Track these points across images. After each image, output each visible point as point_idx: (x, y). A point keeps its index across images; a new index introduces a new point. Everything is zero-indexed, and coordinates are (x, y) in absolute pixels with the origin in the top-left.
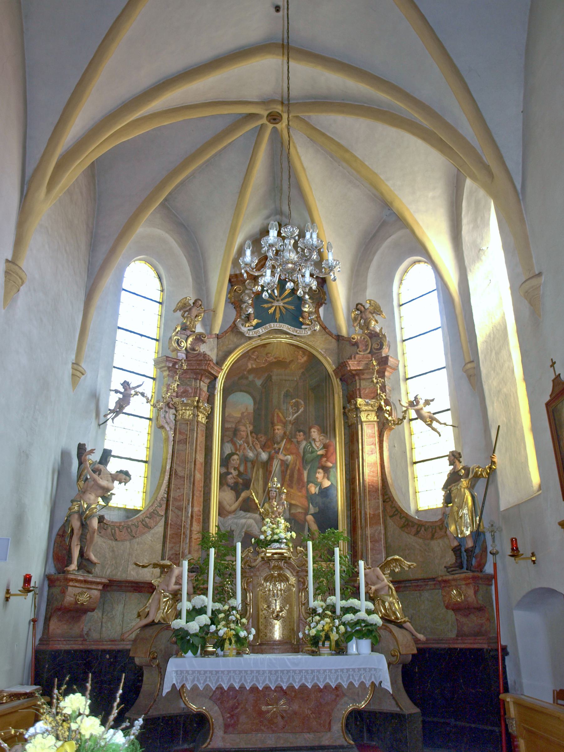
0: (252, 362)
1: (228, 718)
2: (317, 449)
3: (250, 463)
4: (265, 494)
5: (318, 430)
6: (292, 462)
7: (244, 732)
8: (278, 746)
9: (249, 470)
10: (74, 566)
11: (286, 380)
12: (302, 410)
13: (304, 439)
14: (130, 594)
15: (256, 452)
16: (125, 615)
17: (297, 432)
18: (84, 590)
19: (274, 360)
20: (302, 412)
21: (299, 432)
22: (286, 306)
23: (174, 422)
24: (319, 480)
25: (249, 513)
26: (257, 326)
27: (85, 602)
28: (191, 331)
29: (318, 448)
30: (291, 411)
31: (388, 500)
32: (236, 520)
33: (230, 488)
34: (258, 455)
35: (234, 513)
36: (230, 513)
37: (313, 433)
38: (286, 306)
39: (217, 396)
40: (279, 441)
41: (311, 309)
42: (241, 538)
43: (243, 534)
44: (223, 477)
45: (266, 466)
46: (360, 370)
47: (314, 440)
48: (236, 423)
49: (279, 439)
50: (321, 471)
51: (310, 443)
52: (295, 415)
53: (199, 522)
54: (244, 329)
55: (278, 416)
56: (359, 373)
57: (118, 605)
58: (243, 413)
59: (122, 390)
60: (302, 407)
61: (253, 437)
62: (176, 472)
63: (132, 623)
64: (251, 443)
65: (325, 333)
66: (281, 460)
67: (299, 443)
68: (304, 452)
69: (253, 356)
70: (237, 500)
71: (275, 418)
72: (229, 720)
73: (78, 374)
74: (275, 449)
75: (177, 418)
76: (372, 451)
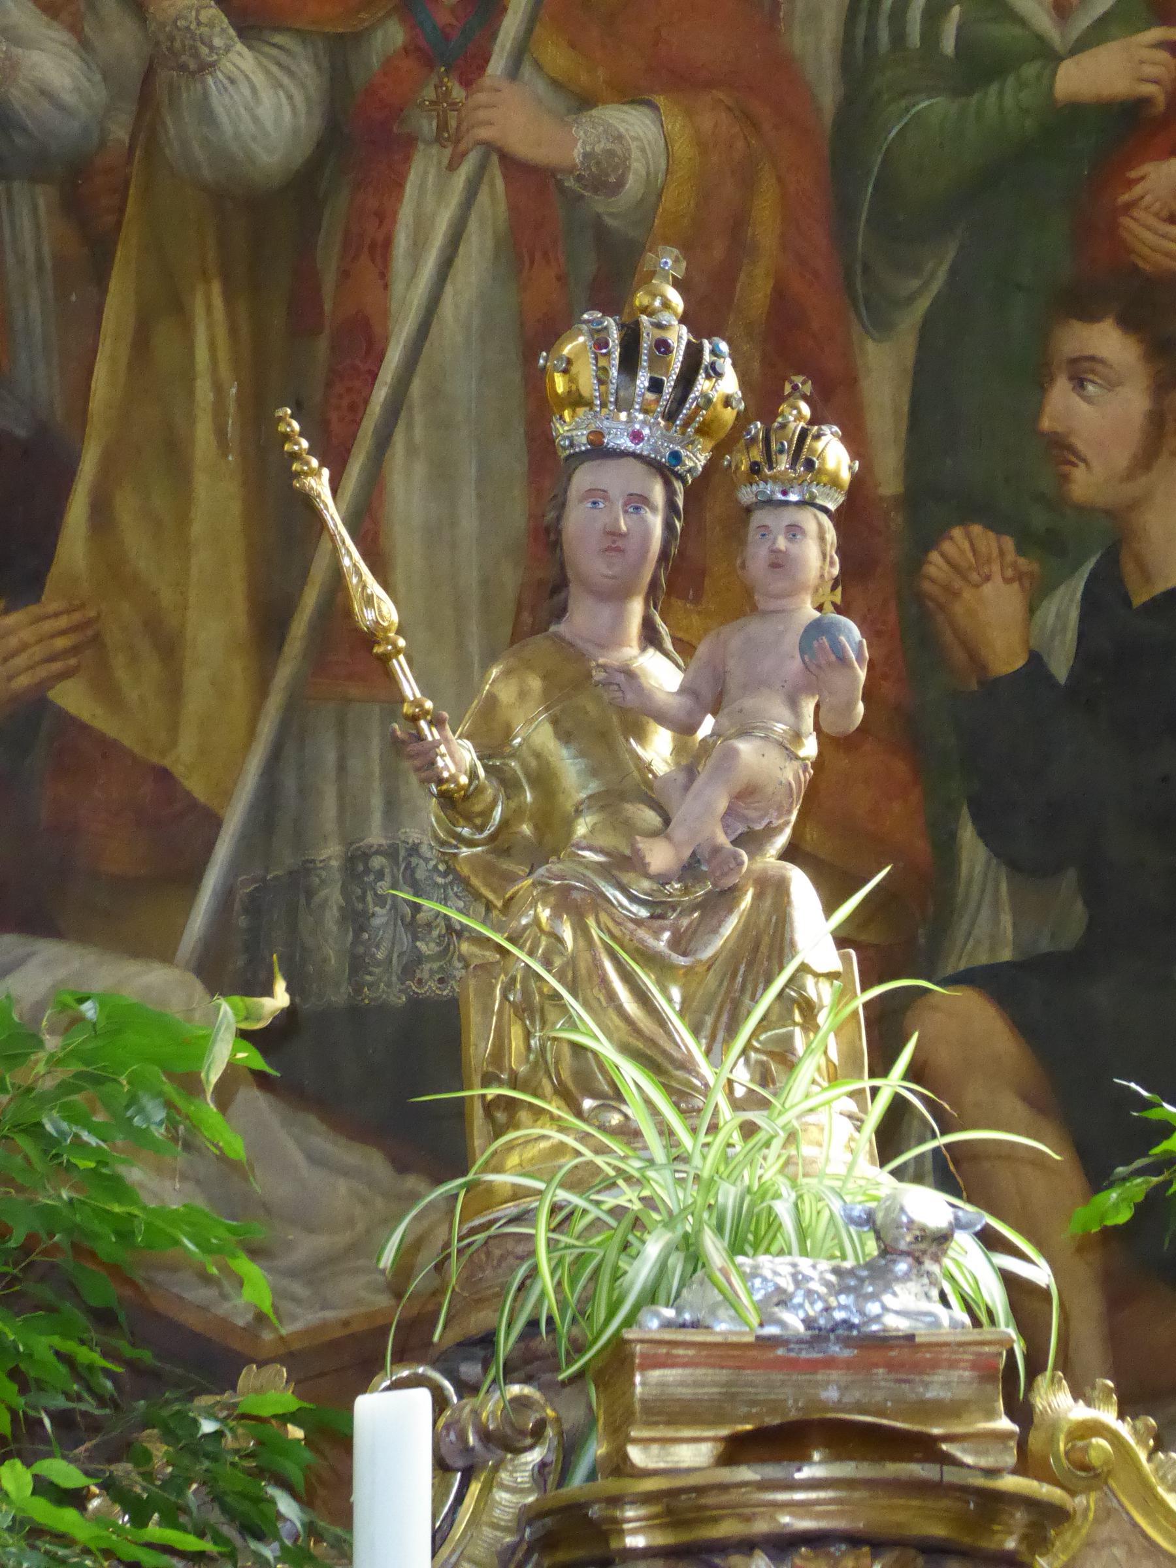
3: (45, 197)
4: (310, 598)
20: (42, 1020)
25: (48, 949)
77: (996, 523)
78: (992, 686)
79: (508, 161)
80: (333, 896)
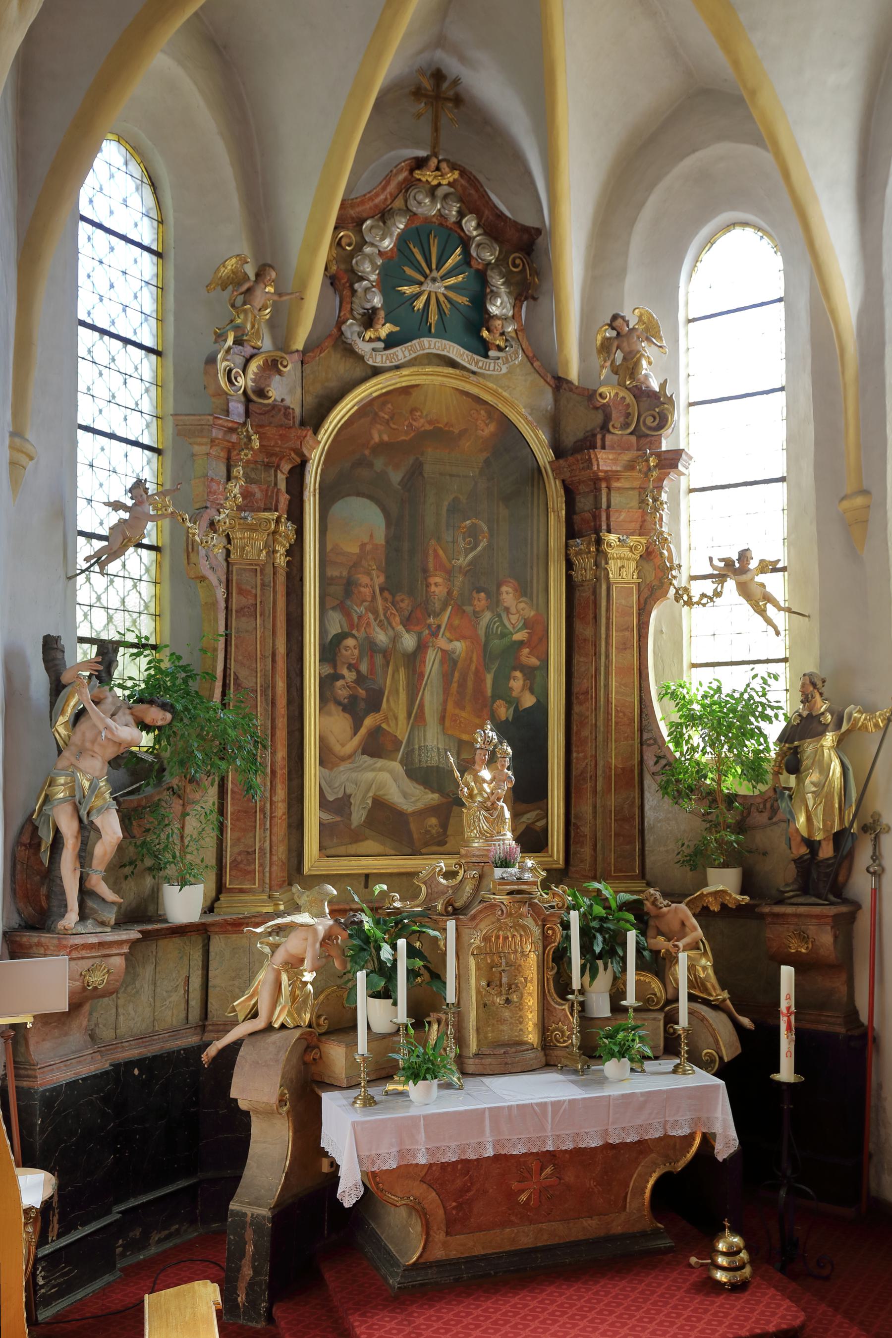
0: (379, 426)
1: (454, 1208)
2: (511, 629)
3: (381, 655)
4: (411, 721)
5: (516, 590)
6: (463, 655)
7: (480, 1229)
8: (539, 1245)
9: (379, 670)
10: (72, 917)
11: (451, 476)
12: (483, 544)
13: (488, 608)
14: (166, 941)
15: (391, 633)
16: (158, 983)
17: (474, 592)
18: (97, 961)
19: (428, 427)
20: (484, 549)
21: (478, 592)
22: (451, 294)
23: (225, 564)
24: (514, 694)
25: (381, 760)
26: (391, 342)
27: (100, 985)
28: (254, 348)
29: (514, 628)
30: (462, 544)
31: (652, 742)
32: (354, 775)
33: (341, 708)
34: (395, 639)
35: (350, 761)
36: (343, 759)
37: (504, 596)
38: (451, 294)
39: (310, 504)
40: (438, 610)
41: (504, 311)
42: (367, 810)
43: (370, 802)
44: (326, 683)
45: (414, 660)
46: (617, 471)
47: (507, 610)
48: (350, 568)
49: (438, 606)
50: (518, 674)
51: (499, 616)
52: (471, 556)
53: (283, 783)
54: (363, 348)
55: (436, 555)
56: (609, 478)
57: (144, 967)
58: (363, 546)
59: (130, 503)
60: (484, 538)
61: (386, 600)
62: (236, 678)
63: (171, 997)
64: (381, 612)
65: (533, 370)
66: (443, 651)
67: (477, 615)
68: (487, 635)
69: (382, 414)
70: (355, 734)
71: (431, 559)
72: (454, 1212)
73: (23, 459)
74: (429, 626)
75: (232, 557)
76: (625, 644)
77: (503, 700)
78: (502, 722)
79: (441, 649)
80: (417, 752)
